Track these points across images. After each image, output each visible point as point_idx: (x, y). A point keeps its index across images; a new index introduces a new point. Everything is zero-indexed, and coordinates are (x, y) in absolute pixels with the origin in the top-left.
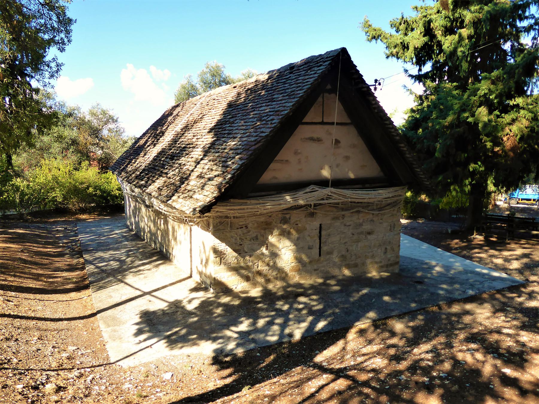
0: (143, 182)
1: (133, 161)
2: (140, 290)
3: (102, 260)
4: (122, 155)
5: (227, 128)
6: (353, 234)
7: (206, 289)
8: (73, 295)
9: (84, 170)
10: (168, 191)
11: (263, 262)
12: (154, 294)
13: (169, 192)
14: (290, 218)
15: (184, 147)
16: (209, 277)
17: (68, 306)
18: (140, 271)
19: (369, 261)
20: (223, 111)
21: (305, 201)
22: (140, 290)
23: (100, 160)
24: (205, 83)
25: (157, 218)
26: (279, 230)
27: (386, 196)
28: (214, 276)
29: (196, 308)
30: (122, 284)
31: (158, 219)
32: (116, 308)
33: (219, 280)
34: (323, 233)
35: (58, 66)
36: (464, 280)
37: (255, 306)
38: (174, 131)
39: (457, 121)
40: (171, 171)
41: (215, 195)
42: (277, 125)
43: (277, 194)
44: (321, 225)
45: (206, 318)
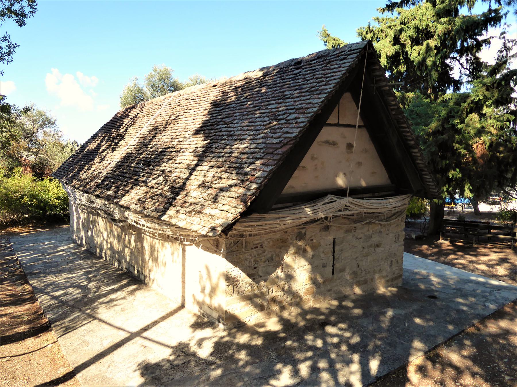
0: (110, 193)
1: (86, 167)
2: (124, 330)
3: (57, 286)
4: (67, 160)
5: (224, 130)
6: (363, 248)
7: (211, 324)
8: (30, 342)
9: (16, 177)
10: (157, 204)
11: (278, 286)
12: (145, 334)
13: (159, 205)
14: (305, 233)
15: (161, 152)
16: (218, 309)
17: (28, 363)
18: (112, 301)
19: (377, 276)
20: (207, 111)
21: (325, 213)
22: (124, 330)
23: (34, 167)
24: (152, 87)
25: (123, 234)
26: (295, 248)
27: (395, 205)
28: (225, 309)
29: (212, 354)
30: (96, 322)
31: (125, 235)
32: (100, 361)
33: (232, 312)
34: (337, 248)
35: (9, 46)
36: (471, 291)
37: (283, 345)
38: (139, 134)
39: (441, 128)
40: (150, 179)
41: (240, 210)
42: (305, 125)
43: (294, 205)
44: (334, 239)
45: (231, 370)
